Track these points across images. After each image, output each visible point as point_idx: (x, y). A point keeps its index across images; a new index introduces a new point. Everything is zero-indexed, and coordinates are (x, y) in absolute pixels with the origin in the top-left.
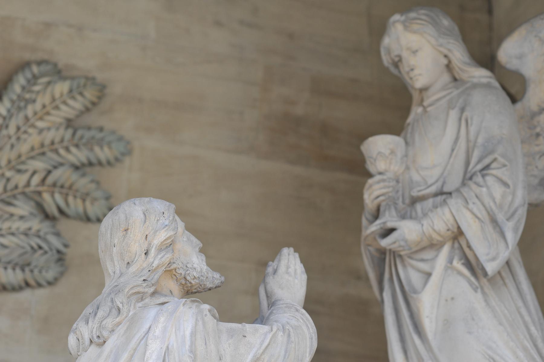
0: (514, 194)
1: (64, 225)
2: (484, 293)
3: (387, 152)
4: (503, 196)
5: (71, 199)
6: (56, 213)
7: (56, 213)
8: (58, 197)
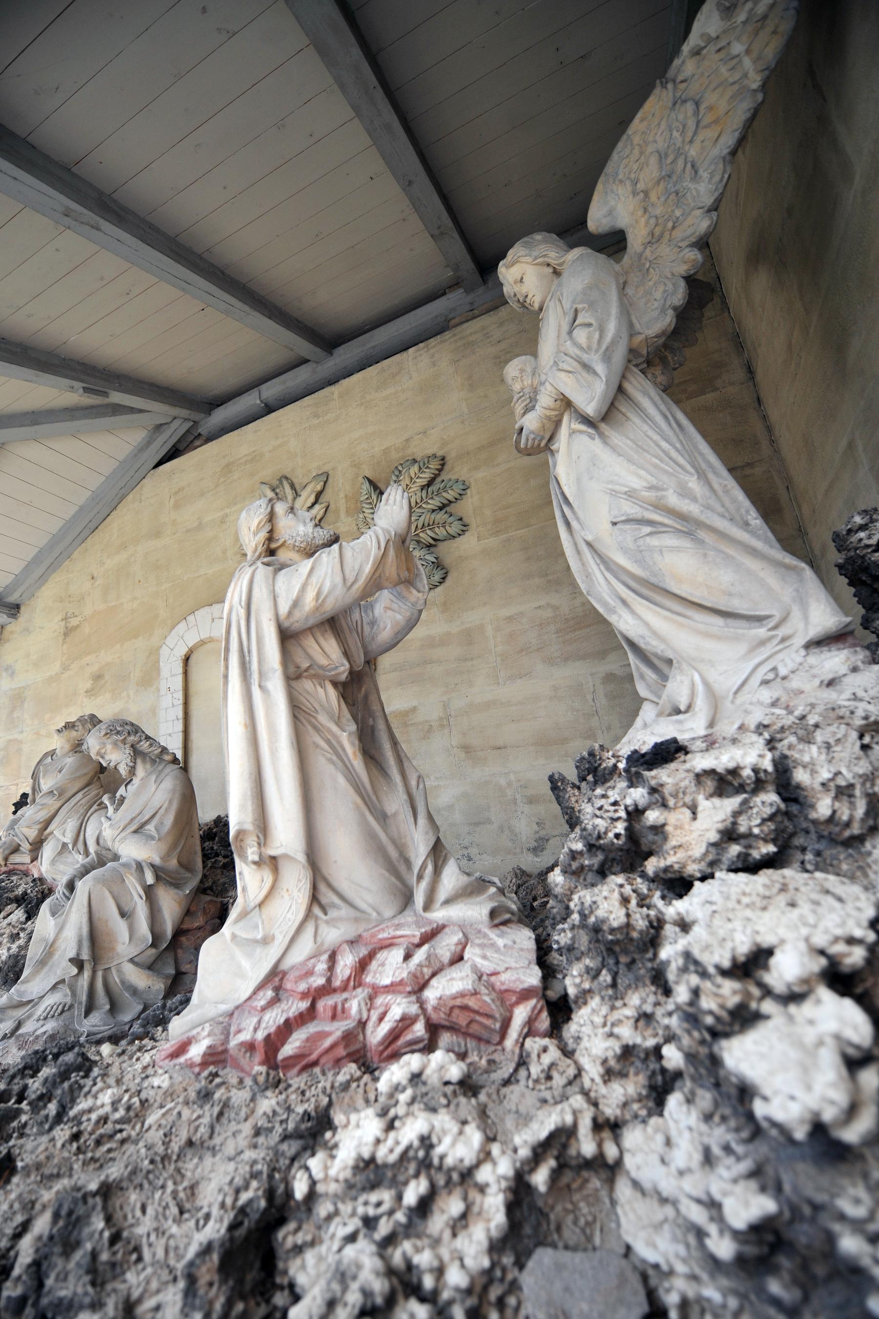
0: (602, 330)
1: (442, 547)
2: (601, 435)
3: (517, 373)
4: (589, 338)
5: (437, 530)
6: (432, 542)
7: (432, 542)
8: (429, 532)
